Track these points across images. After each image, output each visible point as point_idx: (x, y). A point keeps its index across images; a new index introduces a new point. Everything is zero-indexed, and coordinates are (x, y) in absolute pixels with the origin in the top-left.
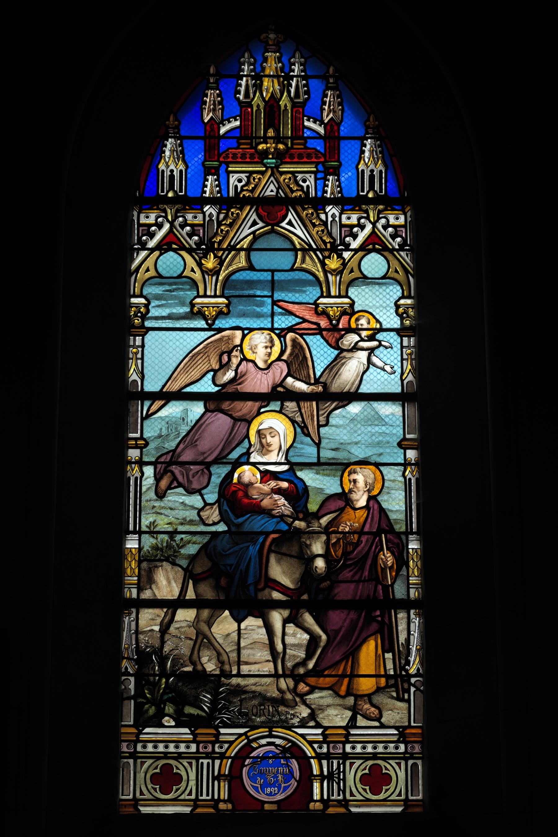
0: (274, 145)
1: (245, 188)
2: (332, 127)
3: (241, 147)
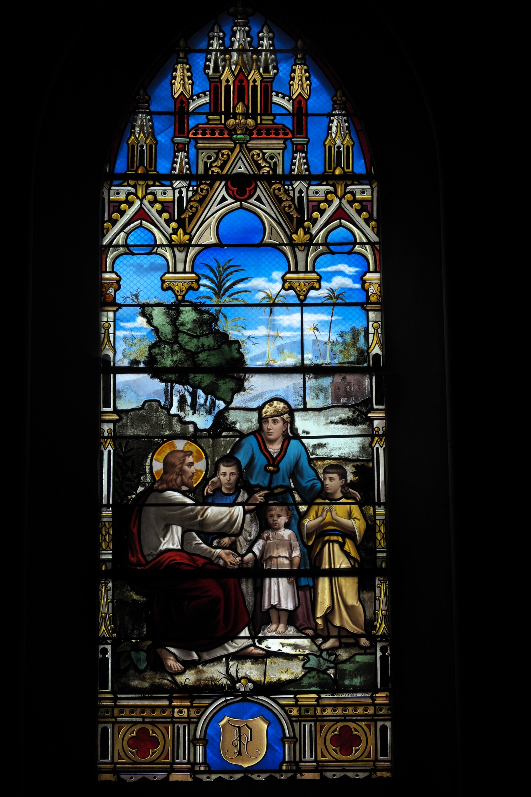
0: (242, 121)
1: (214, 165)
2: (300, 104)
3: (210, 123)
